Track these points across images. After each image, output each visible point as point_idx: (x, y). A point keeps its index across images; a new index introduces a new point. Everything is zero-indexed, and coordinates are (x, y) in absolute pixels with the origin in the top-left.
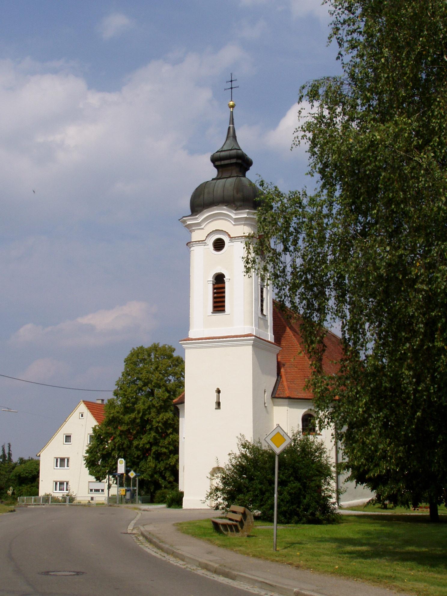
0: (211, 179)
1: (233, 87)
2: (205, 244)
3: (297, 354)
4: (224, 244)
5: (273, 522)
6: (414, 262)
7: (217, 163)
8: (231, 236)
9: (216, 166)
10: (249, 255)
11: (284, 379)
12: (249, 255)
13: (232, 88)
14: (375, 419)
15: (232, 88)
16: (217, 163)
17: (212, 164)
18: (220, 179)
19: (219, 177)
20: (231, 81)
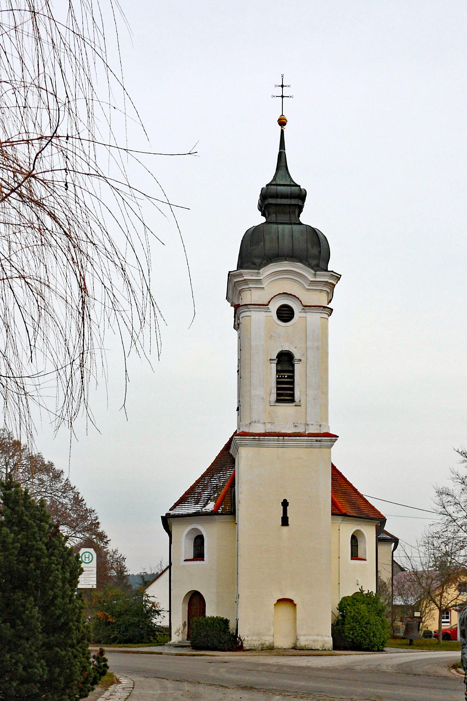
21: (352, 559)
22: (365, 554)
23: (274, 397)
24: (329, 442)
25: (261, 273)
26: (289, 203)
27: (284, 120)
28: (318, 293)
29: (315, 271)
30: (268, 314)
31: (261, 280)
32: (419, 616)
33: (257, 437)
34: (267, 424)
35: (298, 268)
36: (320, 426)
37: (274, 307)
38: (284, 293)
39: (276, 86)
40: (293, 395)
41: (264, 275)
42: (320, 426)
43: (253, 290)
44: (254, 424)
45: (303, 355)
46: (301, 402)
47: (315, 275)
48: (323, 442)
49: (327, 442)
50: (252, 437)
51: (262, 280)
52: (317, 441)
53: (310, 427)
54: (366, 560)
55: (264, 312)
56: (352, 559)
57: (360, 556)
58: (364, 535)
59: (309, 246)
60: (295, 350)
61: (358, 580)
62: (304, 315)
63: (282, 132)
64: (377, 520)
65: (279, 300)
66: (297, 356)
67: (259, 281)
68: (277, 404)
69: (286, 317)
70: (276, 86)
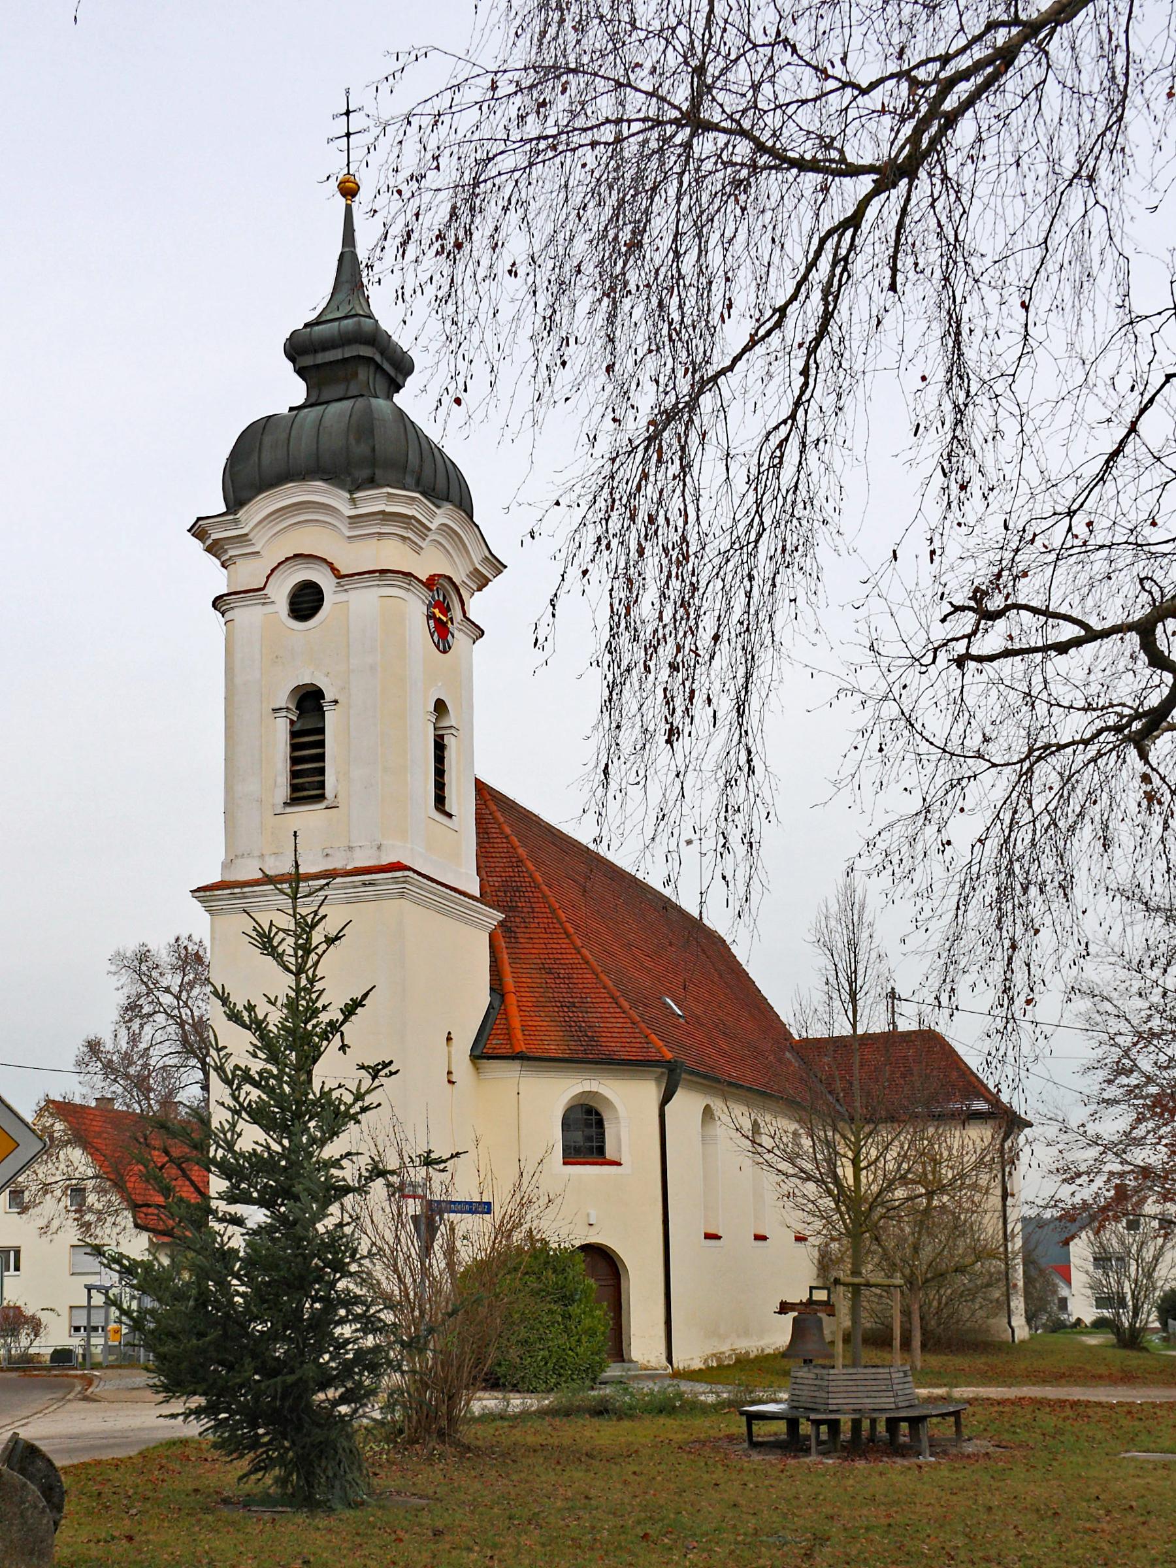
0: (301, 327)
1: (351, 131)
2: (267, 602)
3: (834, 379)
4: (322, 600)
5: (890, 1345)
6: (392, 1338)
7: (307, 361)
8: (343, 572)
9: (300, 372)
10: (181, 1418)
11: (512, 999)
12: (181, 1418)
13: (348, 135)
14: (560, 1375)
15: (348, 135)
16: (307, 361)
17: (290, 365)
18: (312, 405)
19: (312, 400)
20: (348, 113)
21: (565, 1163)
22: (619, 1151)
23: (283, 791)
24: (392, 883)
25: (243, 519)
26: (340, 357)
27: (351, 185)
28: (374, 541)
29: (351, 492)
30: (269, 609)
31: (246, 535)
32: (825, 1298)
33: (237, 890)
34: (267, 858)
35: (318, 492)
36: (379, 848)
37: (281, 591)
38: (296, 556)
39: (334, 117)
40: (322, 785)
41: (252, 524)
42: (379, 848)
43: (239, 562)
44: (239, 861)
45: (343, 688)
46: (339, 799)
47: (353, 501)
48: (380, 885)
49: (388, 884)
50: (228, 891)
51: (250, 537)
52: (364, 885)
53: (357, 853)
54: (619, 1164)
55: (260, 607)
56: (565, 1163)
57: (610, 1154)
58: (607, 1099)
59: (352, 441)
60: (326, 679)
61: (588, 1215)
62: (343, 597)
63: (349, 210)
64: (658, 1067)
65: (291, 574)
66: (329, 696)
67: (243, 539)
68: (289, 810)
69: (306, 609)
70: (334, 117)
